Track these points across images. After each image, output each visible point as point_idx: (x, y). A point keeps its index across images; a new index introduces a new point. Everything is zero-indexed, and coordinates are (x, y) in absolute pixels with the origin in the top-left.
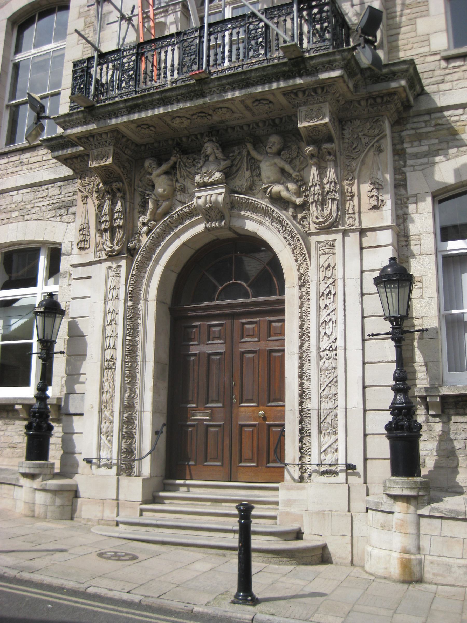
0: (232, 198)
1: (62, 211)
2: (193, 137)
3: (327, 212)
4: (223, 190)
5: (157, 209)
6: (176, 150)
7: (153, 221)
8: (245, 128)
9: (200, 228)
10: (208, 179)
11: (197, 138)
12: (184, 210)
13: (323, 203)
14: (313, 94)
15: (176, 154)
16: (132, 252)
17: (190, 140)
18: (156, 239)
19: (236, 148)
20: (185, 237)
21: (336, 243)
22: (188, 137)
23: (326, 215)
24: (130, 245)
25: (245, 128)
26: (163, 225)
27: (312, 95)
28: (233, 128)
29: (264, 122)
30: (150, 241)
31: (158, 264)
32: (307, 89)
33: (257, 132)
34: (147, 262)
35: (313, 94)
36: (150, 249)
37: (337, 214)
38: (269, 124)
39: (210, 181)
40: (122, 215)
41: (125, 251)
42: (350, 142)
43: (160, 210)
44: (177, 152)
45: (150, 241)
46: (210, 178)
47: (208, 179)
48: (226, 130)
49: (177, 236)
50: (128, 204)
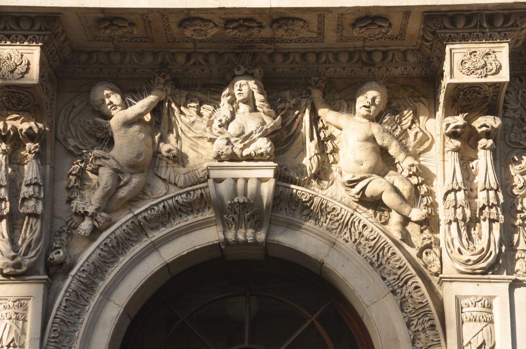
0: (281, 189)
2: (201, 59)
3: (481, 244)
4: (270, 174)
5: (119, 188)
6: (164, 77)
7: (104, 211)
8: (312, 58)
9: (211, 235)
10: (242, 149)
11: (207, 61)
12: (179, 198)
13: (471, 223)
14: (485, 25)
15: (164, 84)
16: (52, 270)
17: (191, 62)
18: (112, 249)
19: (287, 94)
20: (172, 251)
21: (496, 303)
22: (189, 56)
23: (479, 248)
24: (55, 256)
25: (312, 58)
26: (129, 223)
27: (482, 27)
28: (286, 55)
29: (351, 54)
30: (99, 251)
31: (108, 300)
32: (476, 14)
33: (331, 70)
34: (86, 295)
35: (485, 25)
36: (96, 268)
37: (500, 250)
38: (360, 60)
39: (245, 153)
40: (39, 193)
41: (42, 269)
42: (517, 116)
43: (123, 193)
44: (167, 81)
45: (99, 251)
46: (246, 146)
47: (242, 149)
48: (271, 56)
49: (155, 247)
50: (48, 167)
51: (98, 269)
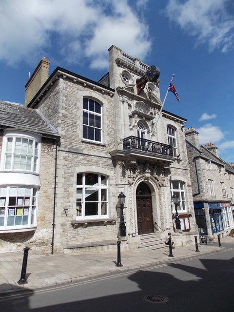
1: (109, 167)
51: (155, 182)
